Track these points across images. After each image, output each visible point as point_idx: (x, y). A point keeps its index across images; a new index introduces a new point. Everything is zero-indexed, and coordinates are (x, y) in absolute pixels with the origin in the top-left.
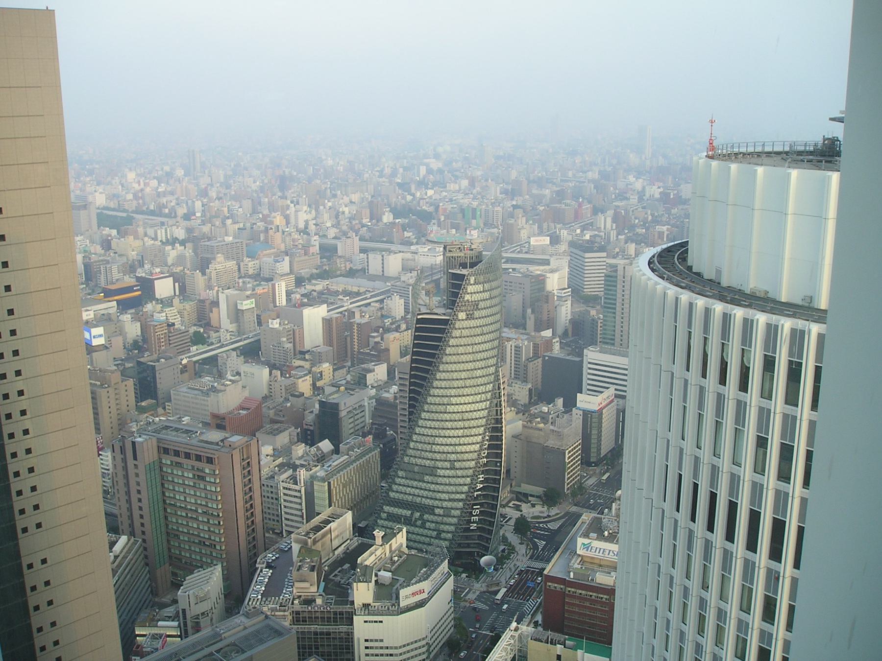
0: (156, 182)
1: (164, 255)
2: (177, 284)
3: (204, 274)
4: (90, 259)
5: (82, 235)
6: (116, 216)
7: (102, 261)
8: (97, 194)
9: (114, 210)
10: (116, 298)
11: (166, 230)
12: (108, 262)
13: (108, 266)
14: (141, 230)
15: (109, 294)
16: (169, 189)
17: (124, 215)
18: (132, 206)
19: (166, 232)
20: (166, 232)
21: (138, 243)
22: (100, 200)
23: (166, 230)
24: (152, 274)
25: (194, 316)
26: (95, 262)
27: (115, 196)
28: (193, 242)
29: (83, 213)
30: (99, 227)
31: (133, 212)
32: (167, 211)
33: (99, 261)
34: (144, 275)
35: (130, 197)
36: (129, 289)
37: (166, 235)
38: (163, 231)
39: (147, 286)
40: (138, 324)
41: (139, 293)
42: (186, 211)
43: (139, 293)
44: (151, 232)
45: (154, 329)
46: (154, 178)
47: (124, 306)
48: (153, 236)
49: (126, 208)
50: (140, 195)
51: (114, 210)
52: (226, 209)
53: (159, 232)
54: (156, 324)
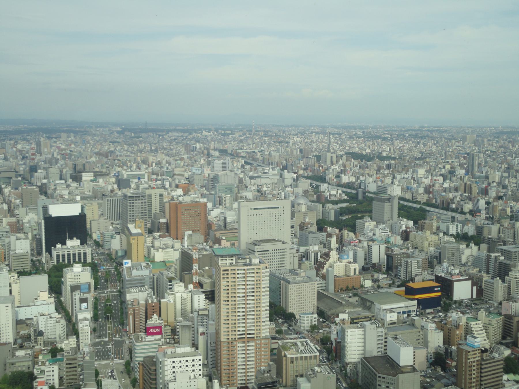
0: (441, 179)
1: (458, 252)
2: (475, 288)
3: (503, 281)
4: (392, 251)
5: (384, 223)
6: (410, 207)
7: (403, 254)
8: (395, 186)
9: (408, 201)
10: (417, 297)
11: (457, 226)
12: (408, 256)
13: (409, 260)
14: (435, 225)
15: (410, 292)
16: (452, 185)
17: (417, 206)
18: (424, 198)
19: (457, 228)
20: (457, 228)
21: (434, 238)
22: (397, 191)
23: (457, 226)
24: (451, 274)
25: (499, 332)
26: (397, 254)
27: (408, 189)
28: (488, 243)
29: (387, 205)
30: (399, 217)
31: (424, 204)
32: (454, 206)
33: (400, 254)
34: (443, 275)
35: (421, 190)
36: (430, 290)
37: (457, 230)
38: (455, 227)
39: (446, 285)
40: (441, 334)
41: (439, 294)
42: (471, 208)
43: (439, 294)
44: (443, 227)
45: (466, 355)
46: (441, 175)
47: (423, 304)
48: (445, 231)
49: (419, 200)
50: (431, 190)
51: (408, 201)
52: (508, 210)
53: (451, 227)
54: (469, 349)
